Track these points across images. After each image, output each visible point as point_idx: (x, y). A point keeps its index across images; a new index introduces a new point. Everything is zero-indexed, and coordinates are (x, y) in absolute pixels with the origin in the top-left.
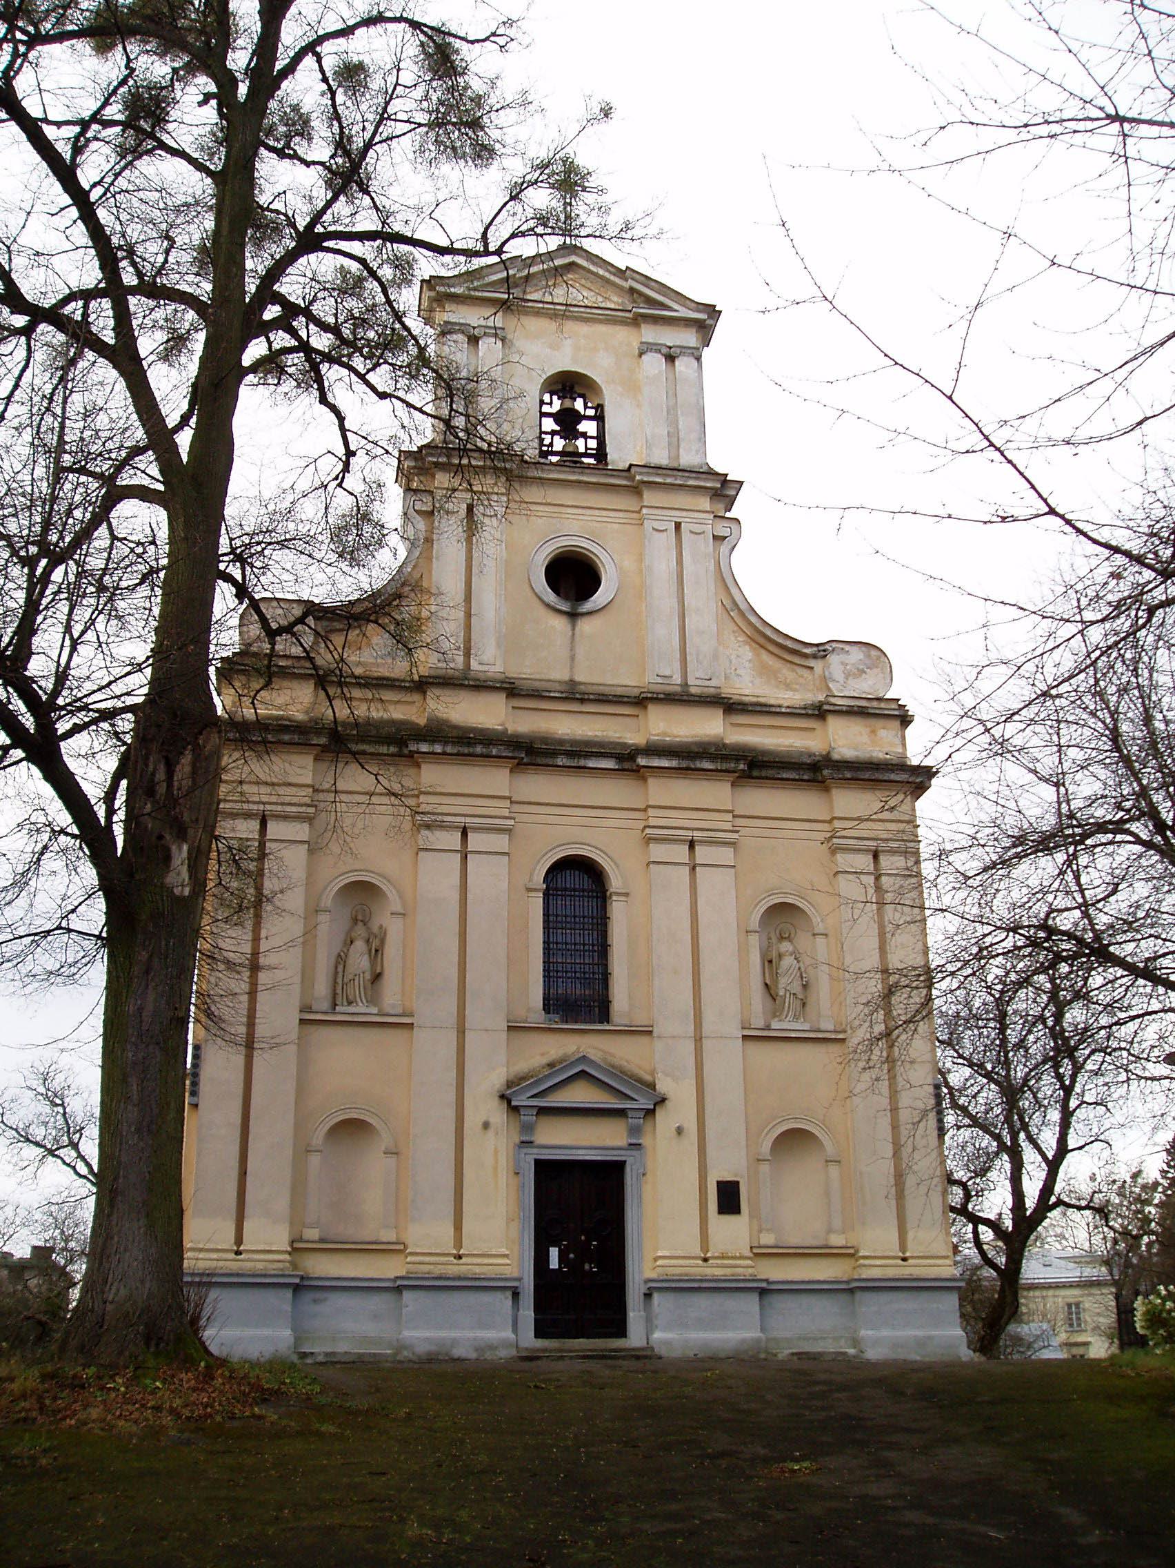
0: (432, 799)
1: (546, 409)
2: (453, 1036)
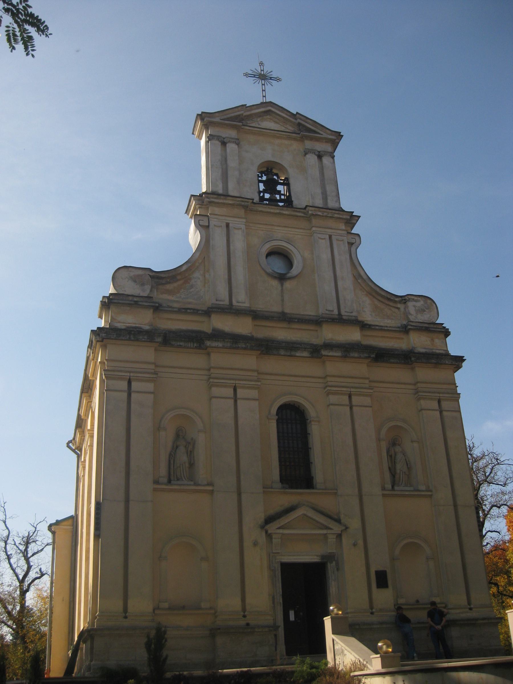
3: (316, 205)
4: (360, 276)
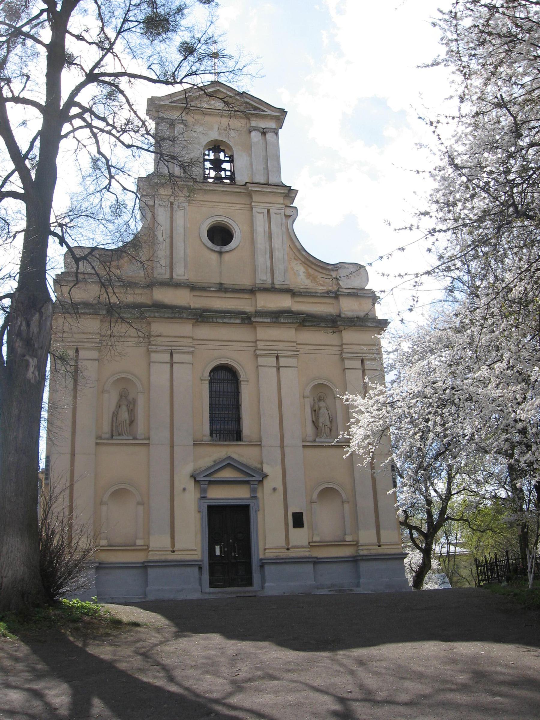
3: (257, 181)
4: (296, 247)
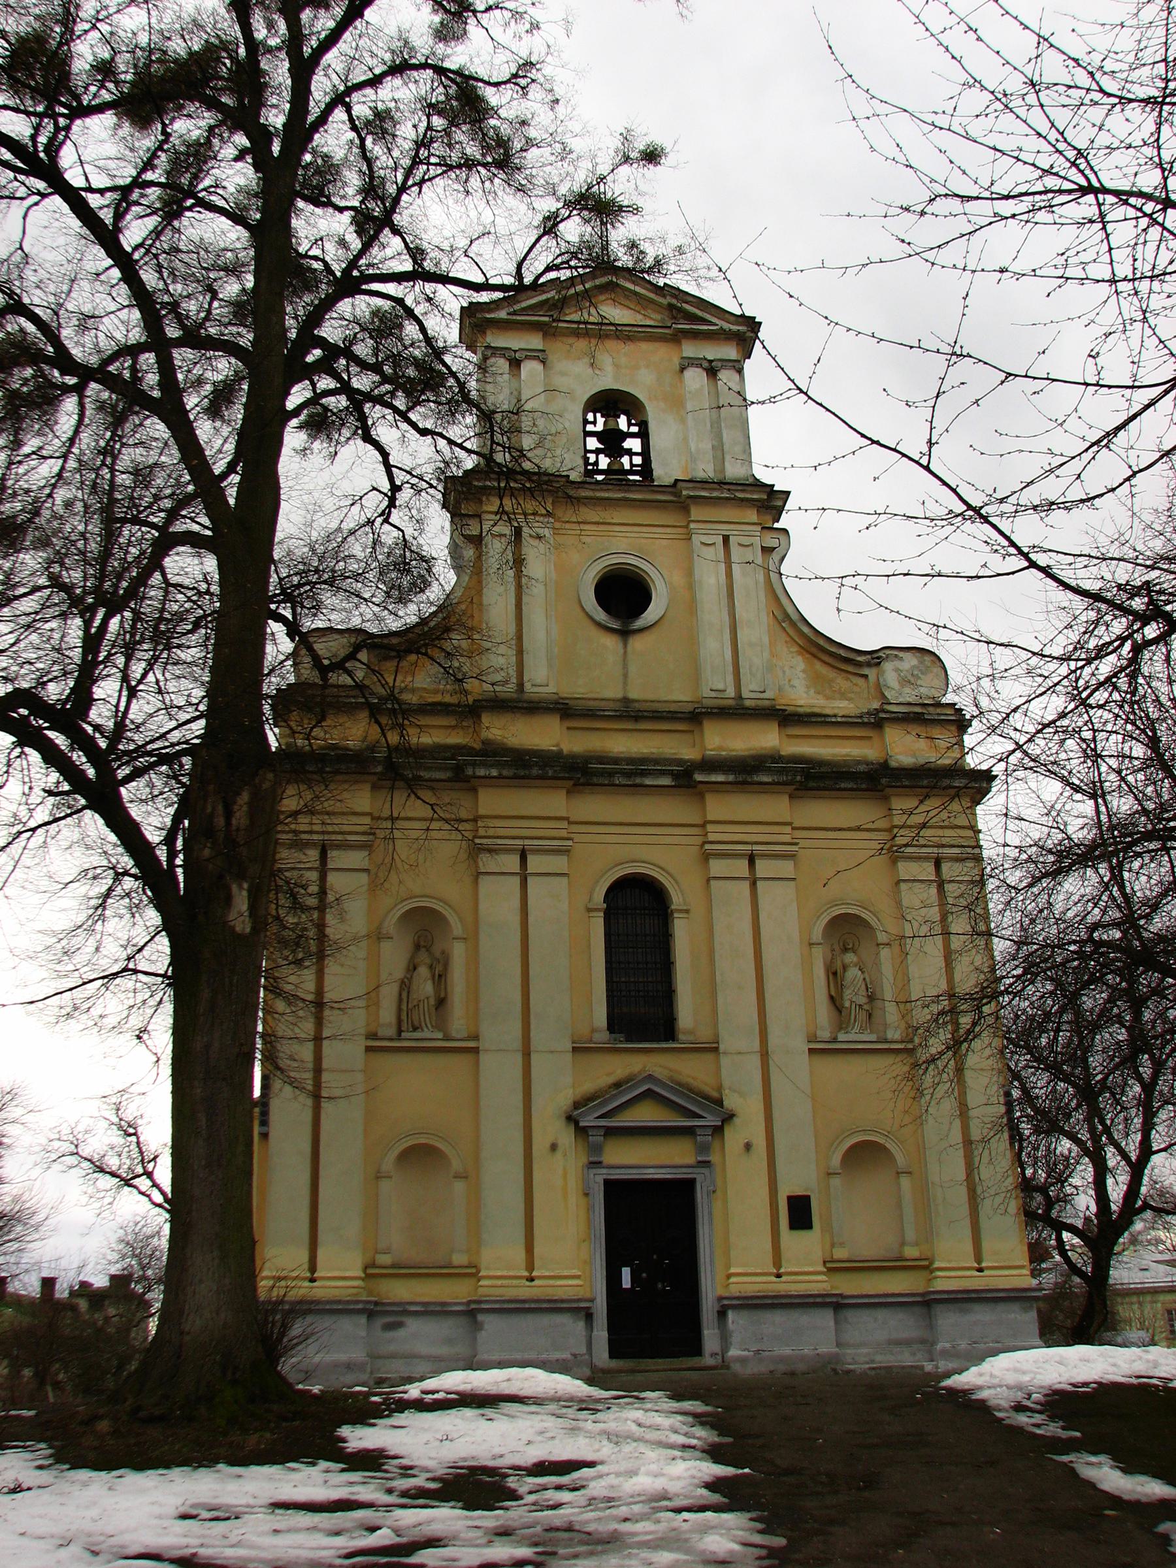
0: (491, 823)
1: (590, 428)
2: (519, 1058)
4: (787, 616)
